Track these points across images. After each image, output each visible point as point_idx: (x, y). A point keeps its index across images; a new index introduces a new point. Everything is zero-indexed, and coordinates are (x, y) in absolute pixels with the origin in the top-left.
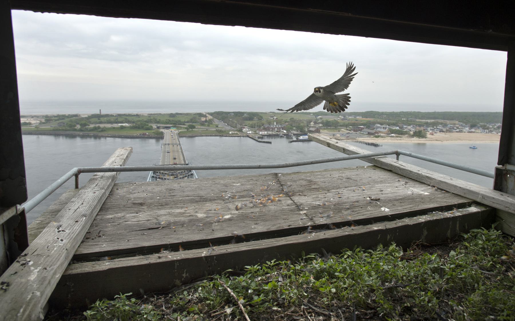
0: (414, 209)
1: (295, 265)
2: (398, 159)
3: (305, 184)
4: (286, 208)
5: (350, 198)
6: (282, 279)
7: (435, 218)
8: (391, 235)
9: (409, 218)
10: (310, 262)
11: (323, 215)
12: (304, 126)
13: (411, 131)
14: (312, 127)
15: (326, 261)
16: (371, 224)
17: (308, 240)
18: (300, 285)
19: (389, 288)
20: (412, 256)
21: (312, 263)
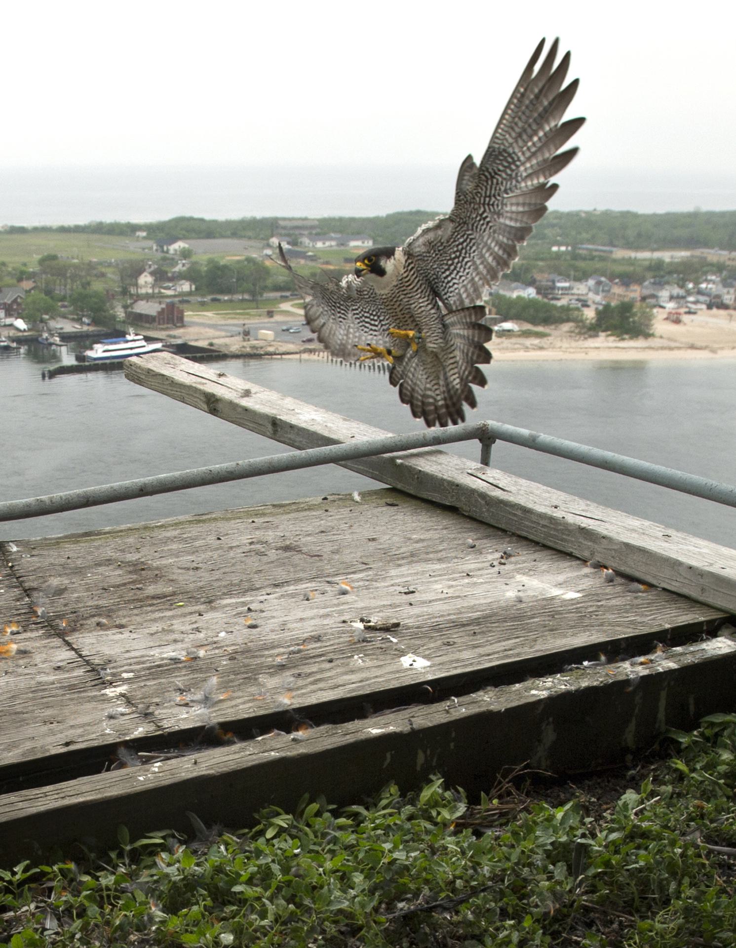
0: (518, 655)
1: (98, 874)
2: (485, 460)
3: (119, 581)
4: (52, 678)
5: (290, 626)
6: (56, 922)
7: (584, 684)
8: (428, 752)
9: (497, 689)
10: (148, 861)
11: (188, 697)
12: (110, 296)
13: (586, 305)
14: (148, 297)
15: (205, 854)
16: (363, 716)
17: (139, 788)
18: (119, 933)
19: (405, 917)
20: (496, 817)
21: (155, 864)
